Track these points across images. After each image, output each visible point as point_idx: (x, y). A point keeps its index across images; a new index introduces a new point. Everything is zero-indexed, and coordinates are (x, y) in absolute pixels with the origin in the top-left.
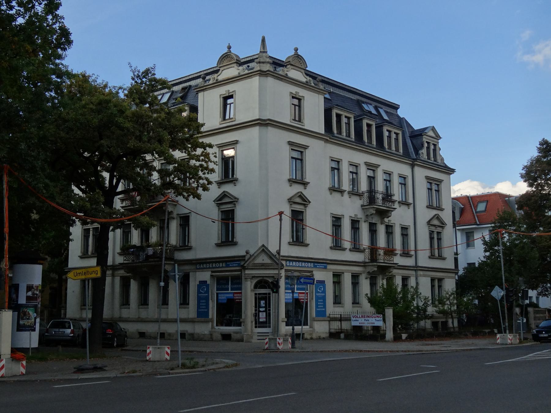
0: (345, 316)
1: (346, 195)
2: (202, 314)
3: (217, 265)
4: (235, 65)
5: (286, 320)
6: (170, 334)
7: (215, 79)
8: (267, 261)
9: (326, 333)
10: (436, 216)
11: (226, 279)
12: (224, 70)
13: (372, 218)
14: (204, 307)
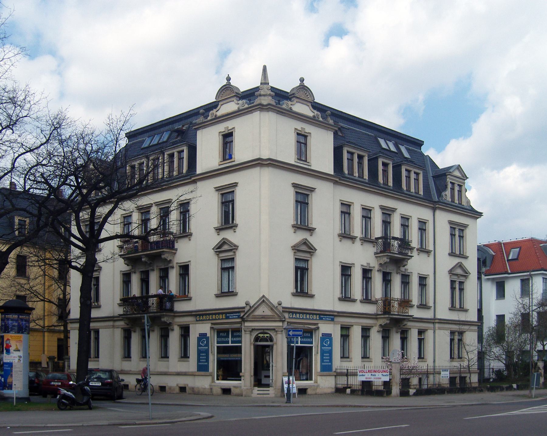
0: (353, 371)
1: (358, 242)
2: (203, 368)
3: (217, 317)
4: (234, 99)
5: (478, 371)
6: (170, 388)
7: (214, 115)
8: (268, 312)
9: (332, 388)
10: (459, 265)
11: (226, 331)
12: (222, 105)
13: (387, 266)
14: (327, 361)
